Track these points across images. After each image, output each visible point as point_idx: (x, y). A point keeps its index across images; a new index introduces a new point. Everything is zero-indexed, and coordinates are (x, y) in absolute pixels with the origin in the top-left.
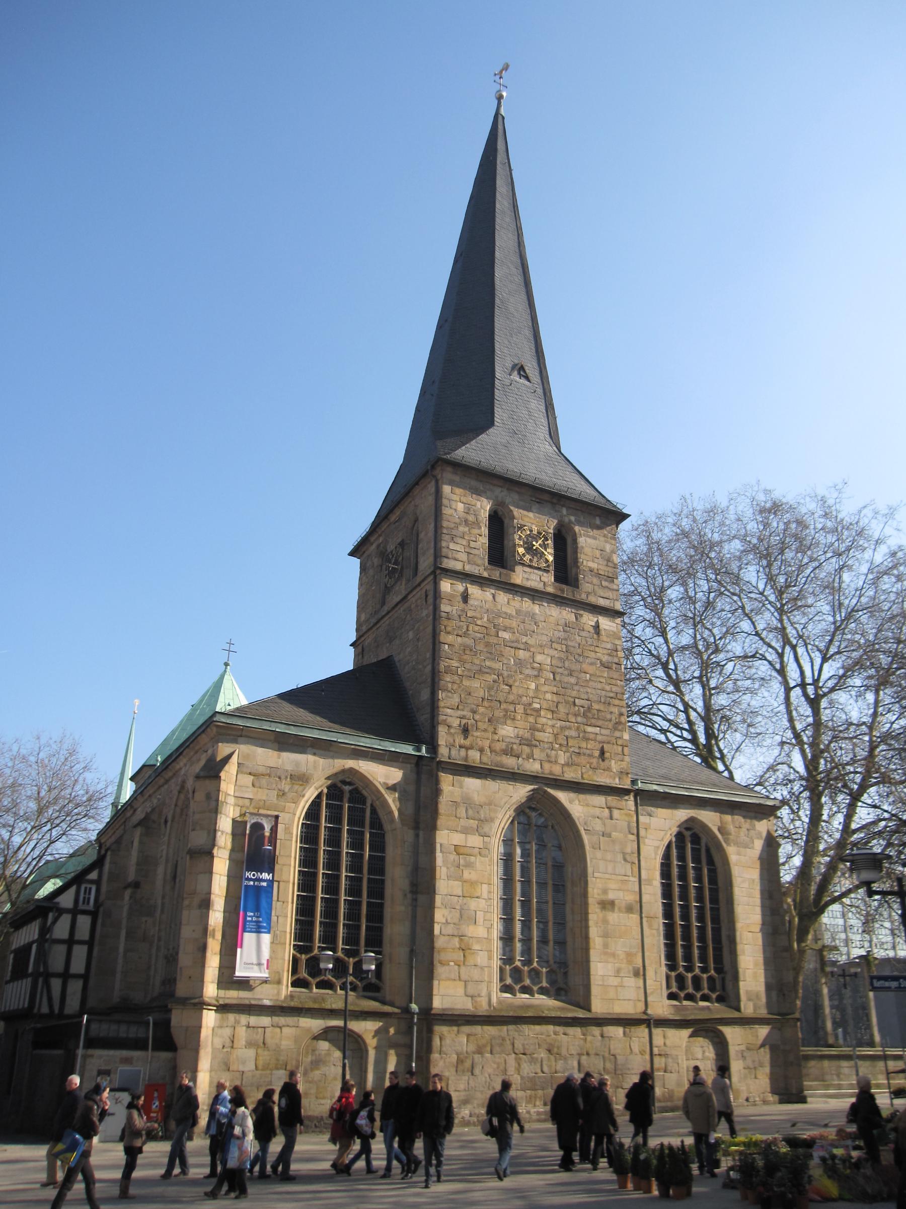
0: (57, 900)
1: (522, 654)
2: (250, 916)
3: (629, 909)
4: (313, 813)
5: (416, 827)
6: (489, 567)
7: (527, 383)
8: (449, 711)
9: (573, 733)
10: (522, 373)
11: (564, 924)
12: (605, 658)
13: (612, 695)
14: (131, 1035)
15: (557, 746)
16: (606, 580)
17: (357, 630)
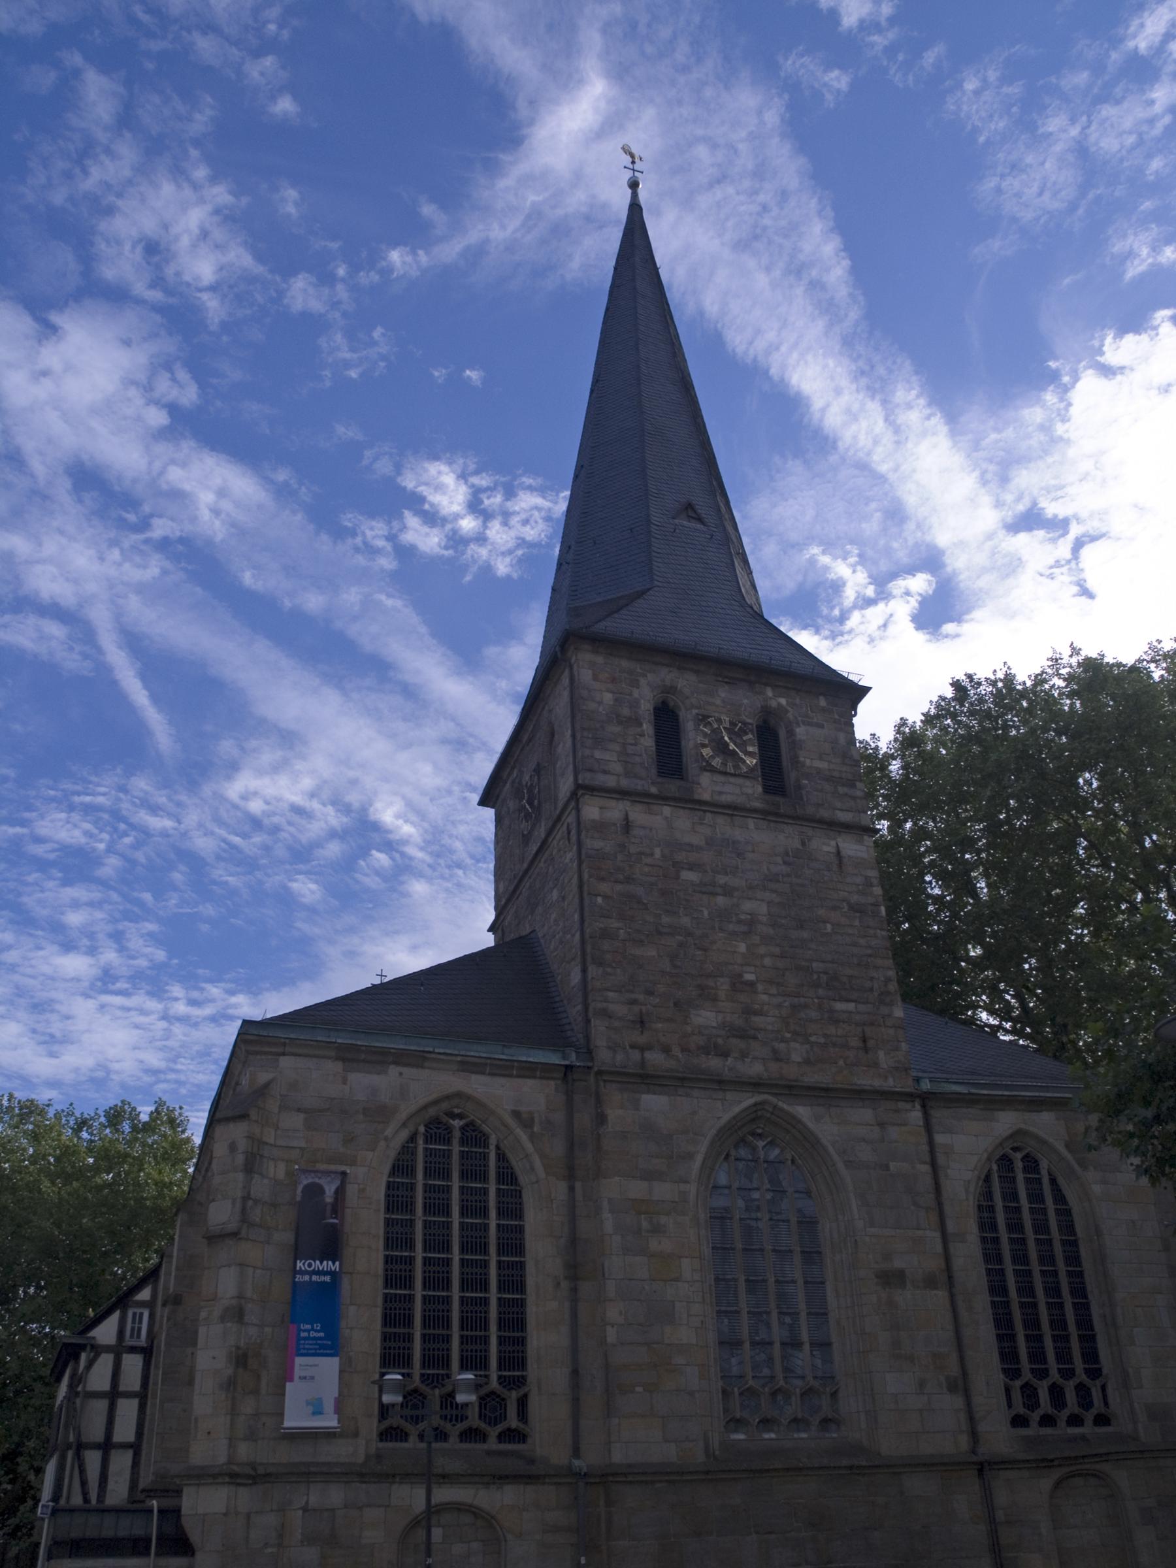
0: (92, 1334)
1: (721, 901)
2: (305, 1331)
3: (930, 1282)
4: (402, 1167)
5: (571, 1174)
6: (660, 780)
7: (699, 526)
8: (611, 994)
9: (814, 1014)
11: (826, 1314)
12: (855, 898)
13: (869, 951)
14: (122, 1533)
15: (788, 1035)
16: (843, 785)
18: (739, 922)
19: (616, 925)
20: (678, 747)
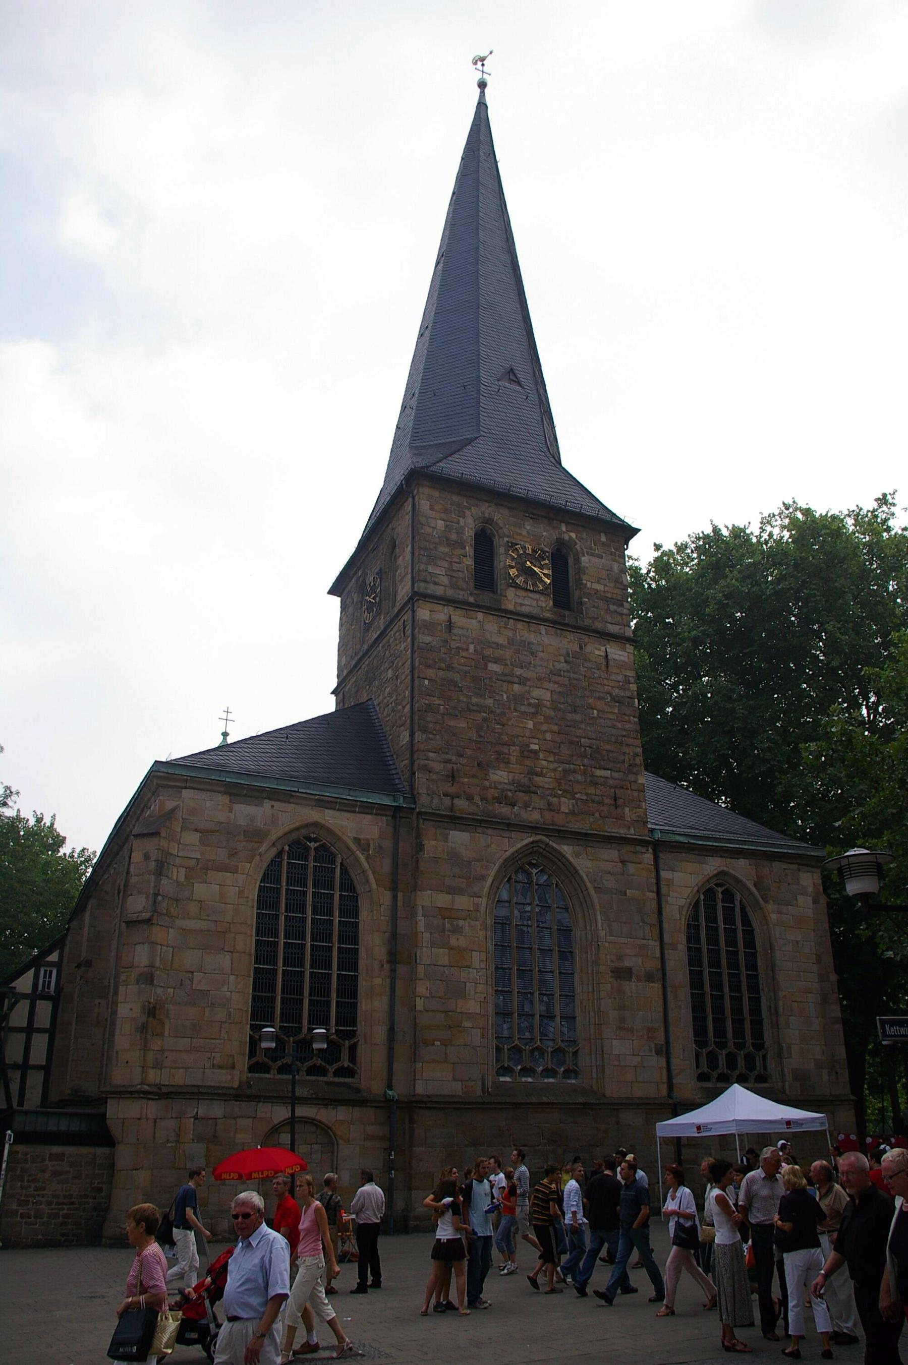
0: (13, 985)
7: (518, 388)
10: (512, 377)
12: (616, 692)
15: (560, 792)
17: (338, 676)
18: (530, 704)
19: (437, 702)
20: (492, 566)
